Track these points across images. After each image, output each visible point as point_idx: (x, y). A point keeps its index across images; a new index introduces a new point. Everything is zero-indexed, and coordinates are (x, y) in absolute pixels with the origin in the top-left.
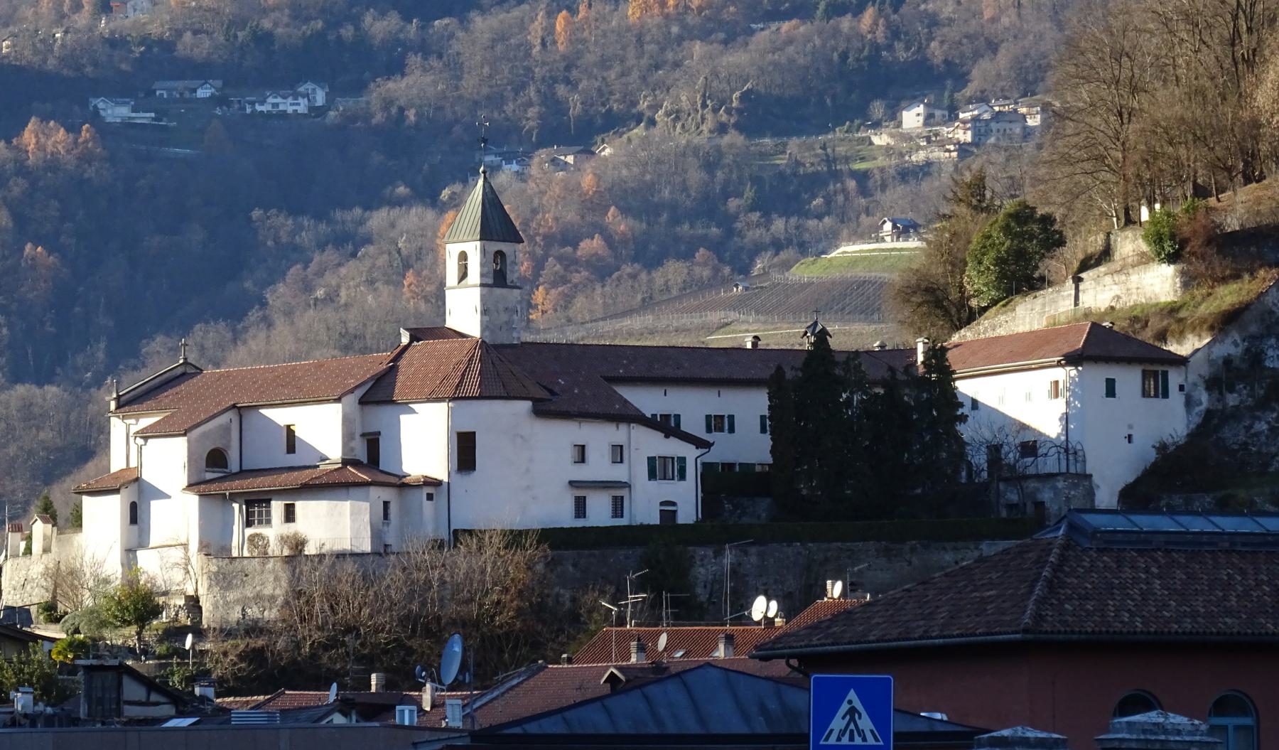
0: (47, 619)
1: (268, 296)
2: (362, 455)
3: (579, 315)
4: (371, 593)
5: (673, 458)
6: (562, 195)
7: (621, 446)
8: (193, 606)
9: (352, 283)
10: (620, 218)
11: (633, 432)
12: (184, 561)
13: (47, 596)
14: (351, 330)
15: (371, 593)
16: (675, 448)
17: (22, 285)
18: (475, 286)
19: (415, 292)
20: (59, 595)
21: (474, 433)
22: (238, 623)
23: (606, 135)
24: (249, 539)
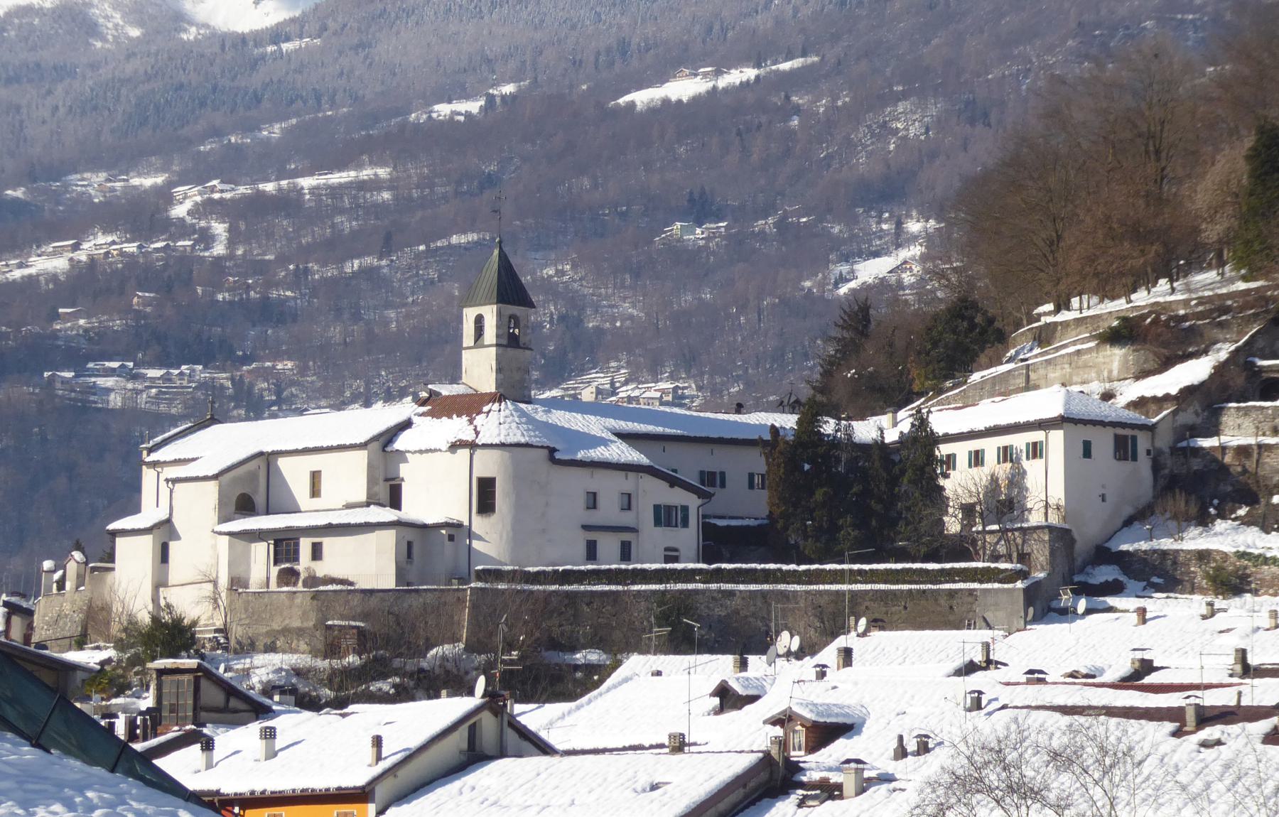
5: (676, 507)
16: (678, 497)
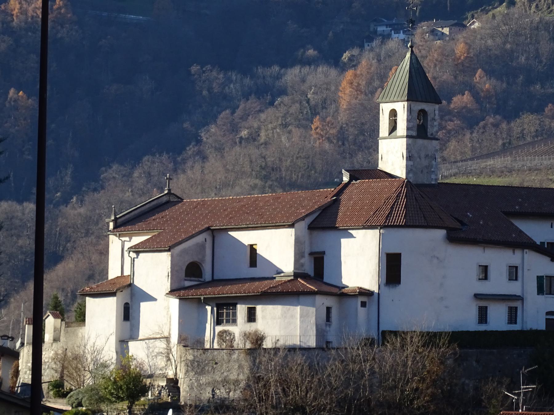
0: (56, 395)
1: (202, 135)
2: (309, 269)
3: (453, 156)
4: (316, 380)
6: (439, 59)
7: (516, 267)
8: (173, 386)
9: (270, 126)
10: (485, 78)
11: (526, 256)
12: (166, 350)
13: (57, 376)
14: (270, 164)
15: (316, 380)
17: (6, 122)
18: (402, 137)
19: (321, 135)
20: (65, 376)
21: (400, 254)
22: (209, 401)
23: (475, 11)
24: (218, 335)
